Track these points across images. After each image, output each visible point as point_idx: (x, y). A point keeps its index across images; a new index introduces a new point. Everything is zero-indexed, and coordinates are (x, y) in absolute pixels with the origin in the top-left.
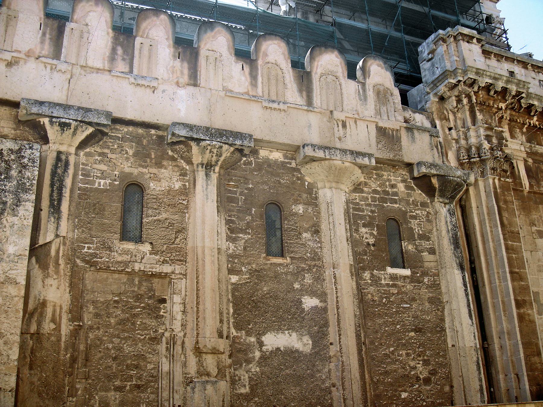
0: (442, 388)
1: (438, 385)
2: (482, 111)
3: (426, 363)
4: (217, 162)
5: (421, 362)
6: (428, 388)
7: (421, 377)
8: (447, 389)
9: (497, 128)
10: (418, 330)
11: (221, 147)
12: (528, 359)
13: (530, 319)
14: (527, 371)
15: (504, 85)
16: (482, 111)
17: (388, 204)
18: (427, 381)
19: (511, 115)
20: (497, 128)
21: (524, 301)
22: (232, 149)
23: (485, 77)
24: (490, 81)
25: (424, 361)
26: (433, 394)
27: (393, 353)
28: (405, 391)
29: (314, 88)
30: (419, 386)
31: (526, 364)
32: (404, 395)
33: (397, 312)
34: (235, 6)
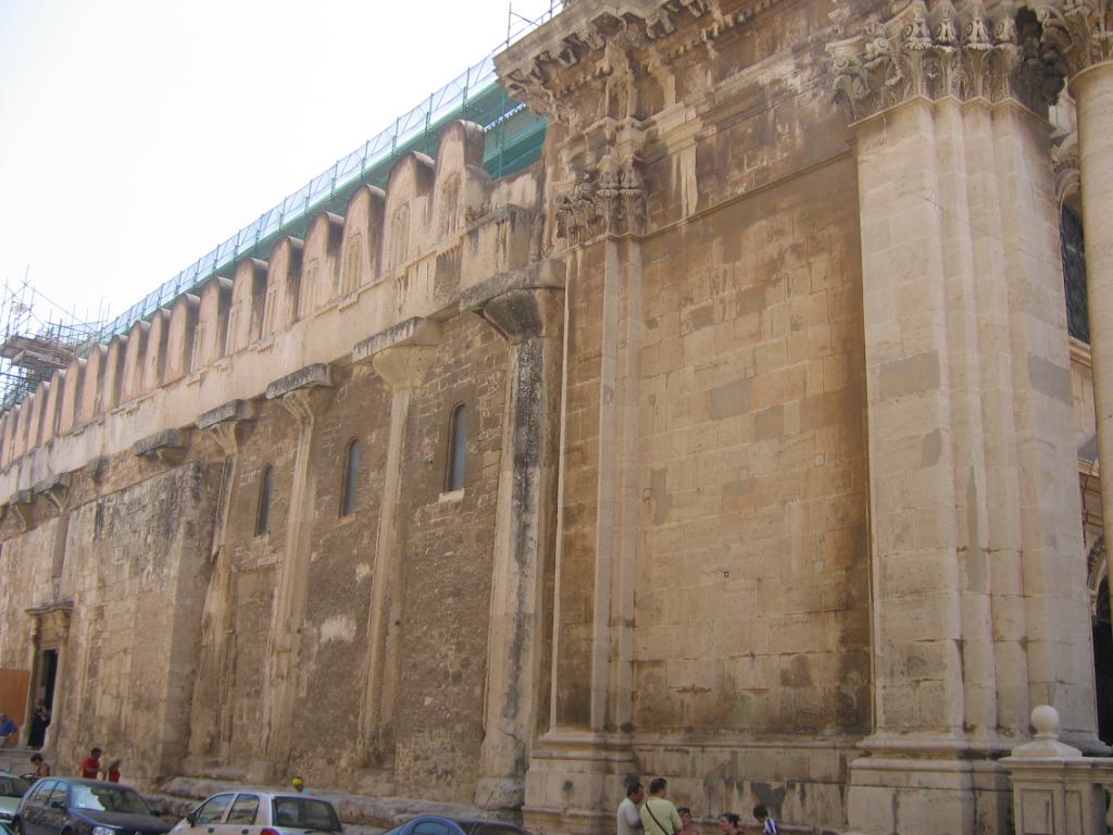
0: (472, 690)
1: (469, 684)
2: (579, 103)
3: (460, 647)
4: (306, 411)
5: (454, 647)
6: (456, 689)
7: (451, 671)
8: (478, 691)
9: (588, 130)
10: (457, 593)
11: (294, 396)
12: (566, 632)
13: (583, 546)
14: (559, 658)
15: (565, 34)
16: (579, 103)
17: (460, 382)
18: (457, 678)
19: (662, 51)
20: (588, 130)
21: (581, 508)
22: (307, 391)
23: (527, 51)
24: (537, 52)
25: (458, 644)
26: (460, 700)
27: (425, 634)
28: (429, 695)
29: (343, 253)
30: (447, 687)
31: (560, 643)
32: (428, 701)
33: (438, 567)
34: (487, 89)
